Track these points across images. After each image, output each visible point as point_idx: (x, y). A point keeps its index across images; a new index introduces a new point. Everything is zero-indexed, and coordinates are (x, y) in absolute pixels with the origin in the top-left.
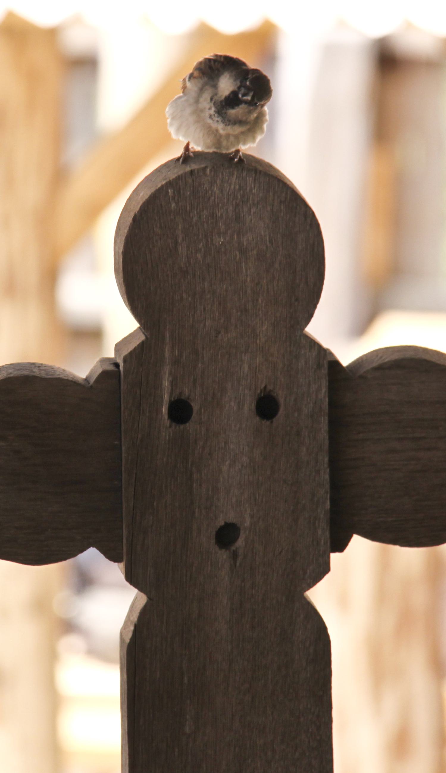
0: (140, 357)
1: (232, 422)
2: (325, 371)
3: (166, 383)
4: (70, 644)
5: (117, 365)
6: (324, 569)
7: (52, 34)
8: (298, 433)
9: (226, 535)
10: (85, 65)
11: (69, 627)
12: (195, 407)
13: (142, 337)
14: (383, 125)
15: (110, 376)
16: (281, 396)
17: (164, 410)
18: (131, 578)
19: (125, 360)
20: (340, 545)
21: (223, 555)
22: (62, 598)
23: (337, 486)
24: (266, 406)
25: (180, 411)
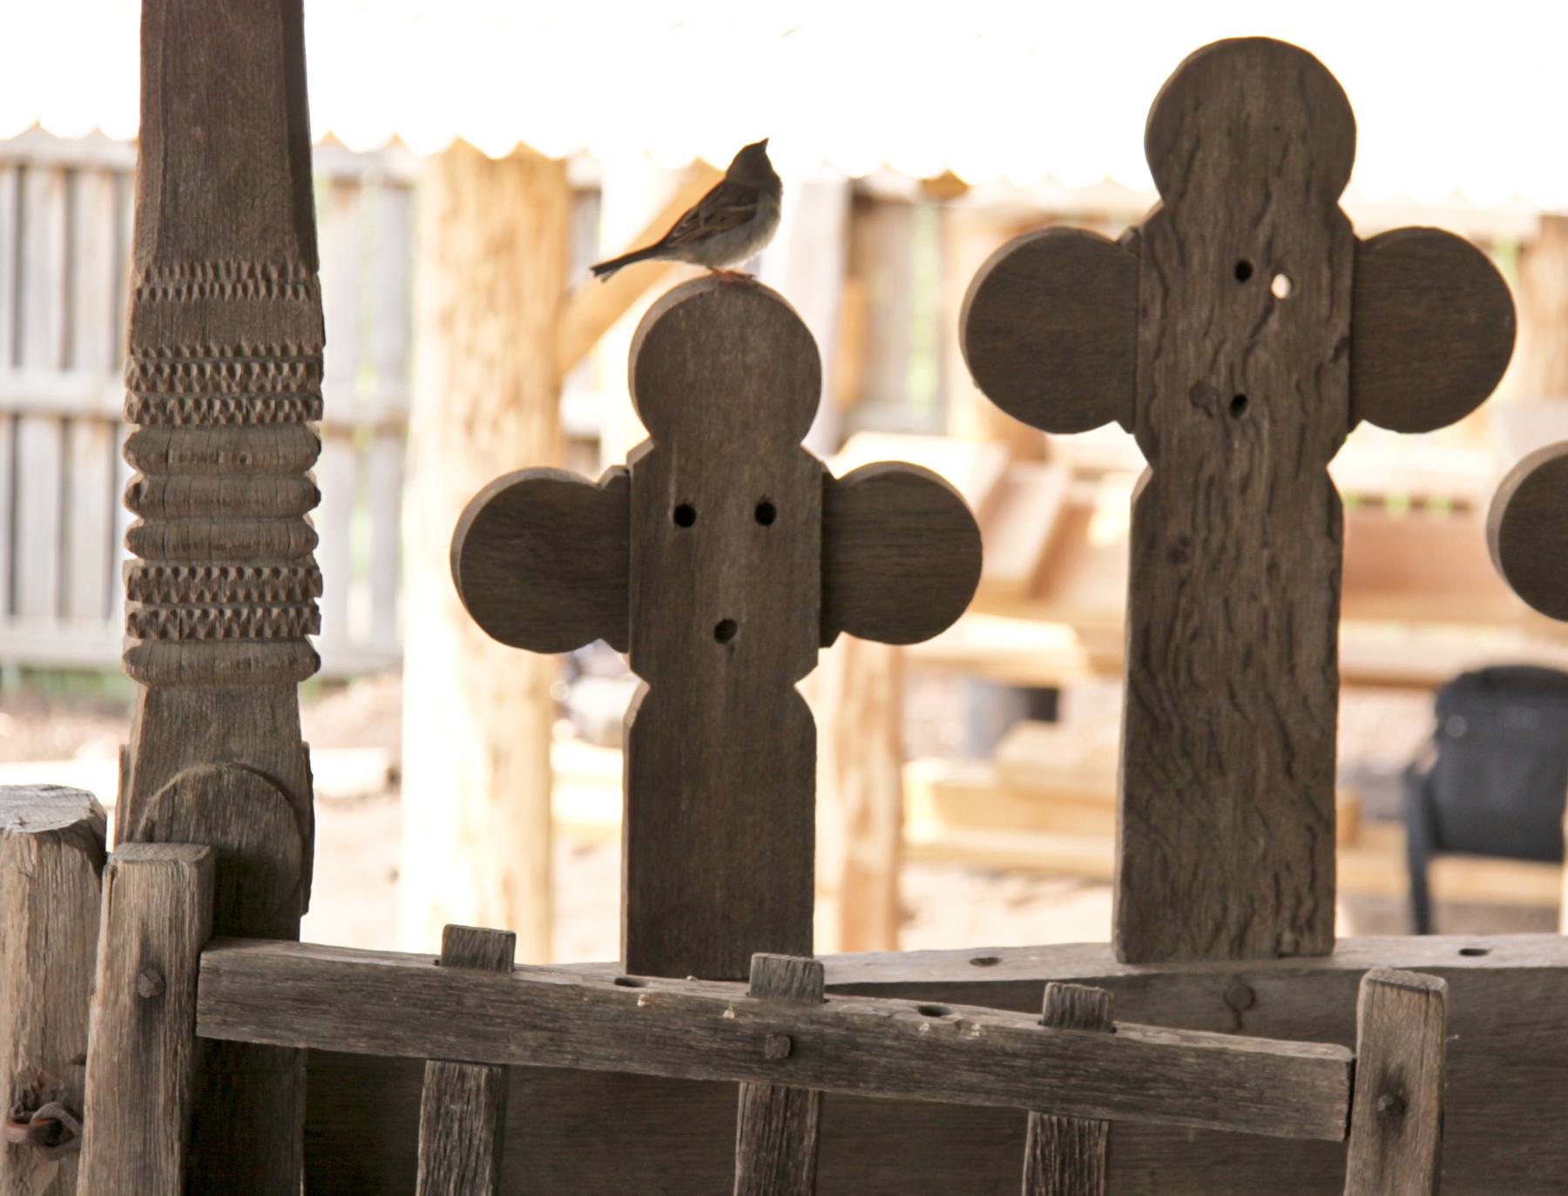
0: (648, 466)
1: (732, 523)
2: (819, 482)
3: (672, 489)
4: (562, 728)
5: (627, 471)
6: (812, 663)
7: (561, 166)
8: (793, 539)
9: (724, 631)
10: (587, 196)
11: (562, 711)
12: (699, 511)
13: (651, 447)
14: (857, 262)
15: (620, 481)
16: (778, 503)
17: (670, 514)
18: (636, 667)
19: (635, 467)
20: (827, 641)
21: (720, 649)
22: (557, 689)
23: (827, 588)
24: (765, 513)
25: (685, 516)
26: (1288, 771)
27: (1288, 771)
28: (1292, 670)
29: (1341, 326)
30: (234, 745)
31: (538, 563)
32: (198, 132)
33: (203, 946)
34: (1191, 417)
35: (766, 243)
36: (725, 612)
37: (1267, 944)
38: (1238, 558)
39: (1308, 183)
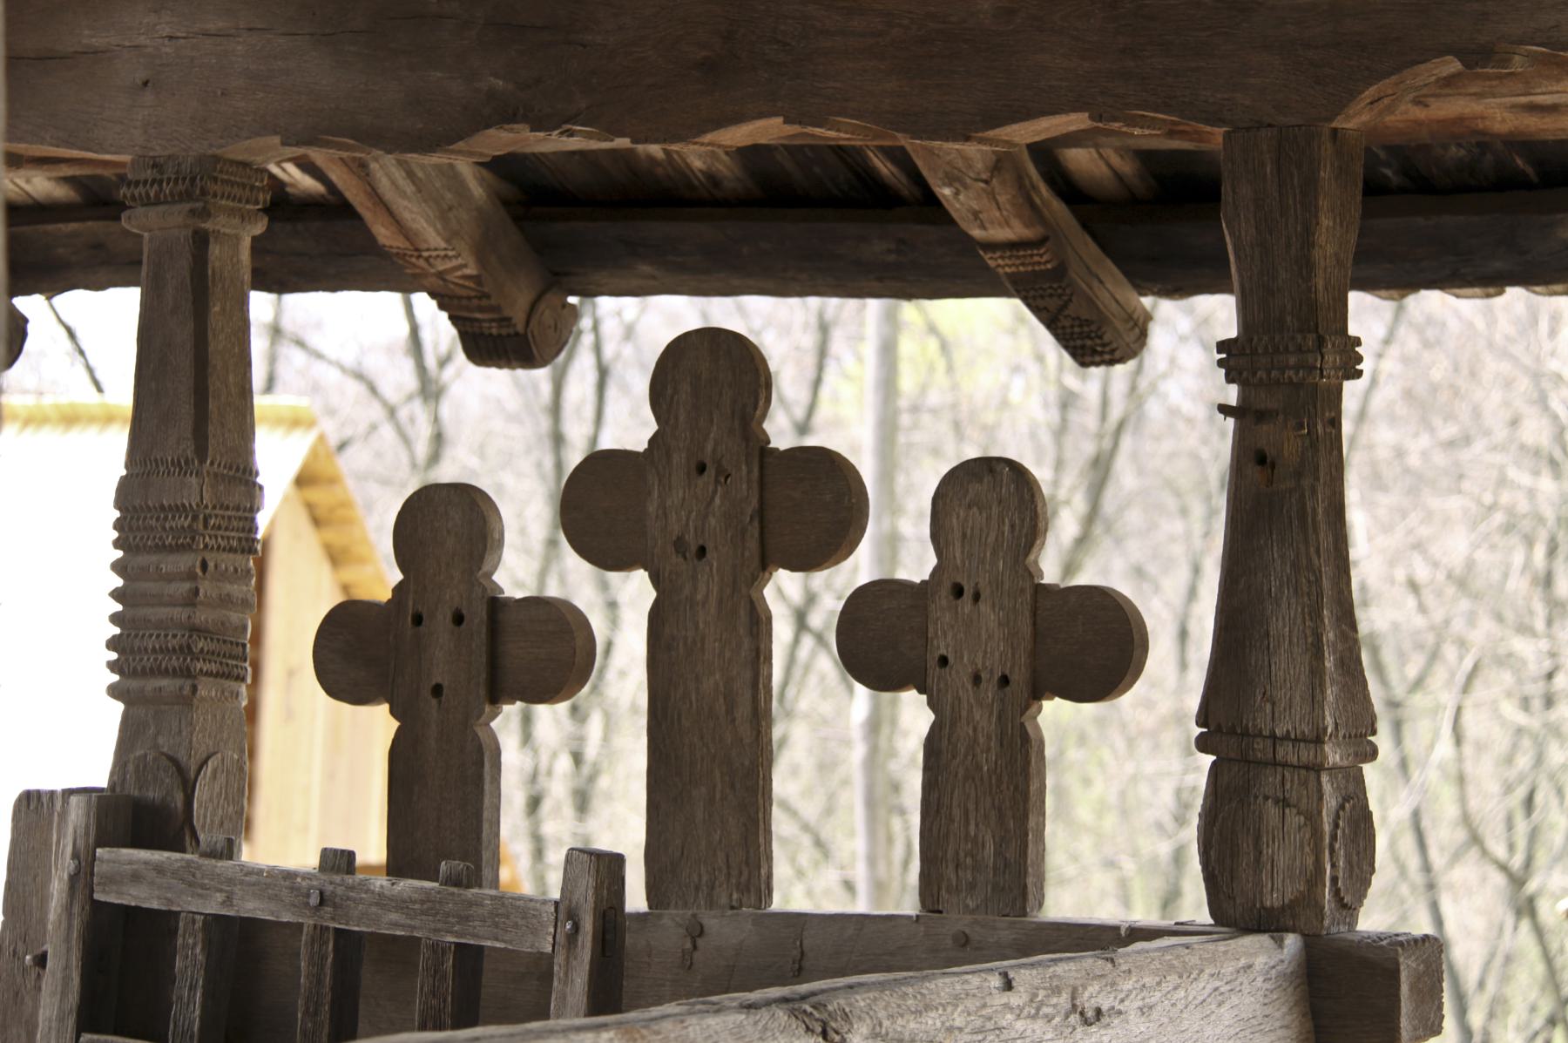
9: (437, 690)
21: (434, 702)
24: (458, 619)
25: (418, 620)
26: (733, 786)
27: (733, 786)
28: (733, 720)
29: (754, 502)
30: (161, 740)
31: (355, 653)
32: (153, 385)
33: (102, 842)
34: (676, 559)
35: (551, 497)
36: (437, 679)
37: (724, 900)
38: (703, 649)
39: (733, 413)
